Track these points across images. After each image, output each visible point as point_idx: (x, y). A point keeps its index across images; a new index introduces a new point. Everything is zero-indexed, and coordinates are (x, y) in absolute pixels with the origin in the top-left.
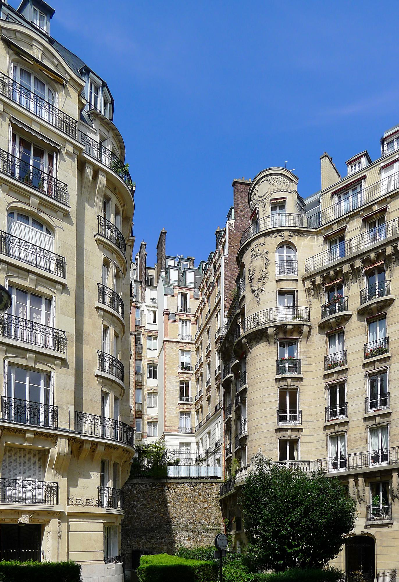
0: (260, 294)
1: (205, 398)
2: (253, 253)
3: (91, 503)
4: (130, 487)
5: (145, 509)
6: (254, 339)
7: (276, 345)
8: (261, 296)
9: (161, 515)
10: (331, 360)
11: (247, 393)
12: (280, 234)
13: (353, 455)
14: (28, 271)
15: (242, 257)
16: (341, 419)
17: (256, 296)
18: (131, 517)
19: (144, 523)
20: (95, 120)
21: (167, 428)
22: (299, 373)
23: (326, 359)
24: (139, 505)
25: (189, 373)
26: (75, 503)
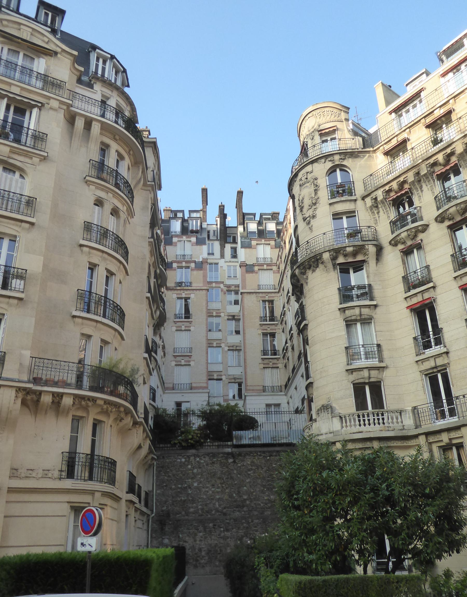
0: (312, 221)
1: (290, 349)
2: (301, 182)
3: (50, 475)
4: (183, 460)
5: (204, 490)
6: (309, 268)
7: (336, 271)
8: (313, 222)
9: (226, 497)
10: (412, 278)
11: (309, 330)
12: (329, 159)
13: (461, 397)
14: (22, 221)
15: (292, 190)
16: (435, 350)
17: (309, 223)
18: (185, 501)
19: (202, 509)
20: (96, 83)
21: (248, 388)
22: (372, 299)
23: (405, 279)
24: (195, 484)
25: (274, 324)
26: (23, 475)
